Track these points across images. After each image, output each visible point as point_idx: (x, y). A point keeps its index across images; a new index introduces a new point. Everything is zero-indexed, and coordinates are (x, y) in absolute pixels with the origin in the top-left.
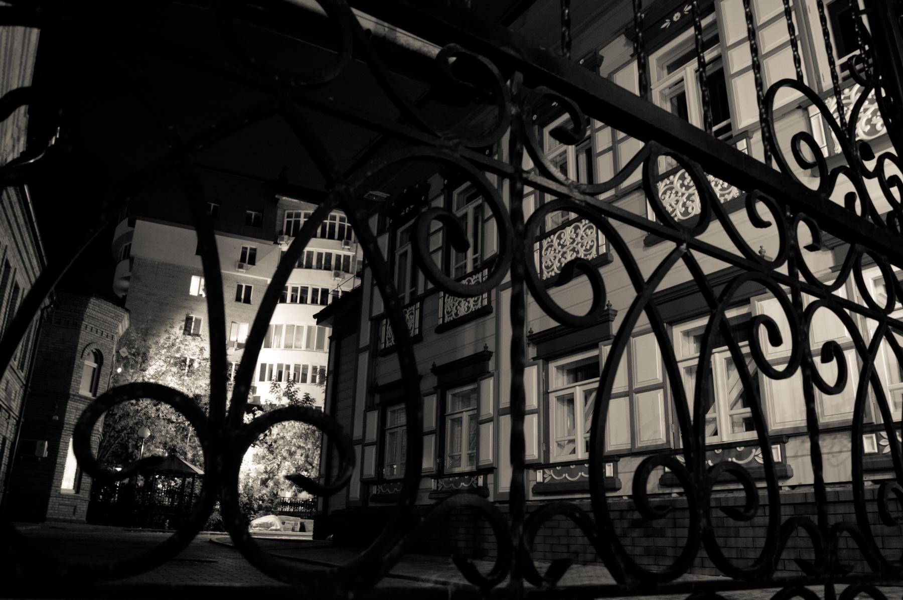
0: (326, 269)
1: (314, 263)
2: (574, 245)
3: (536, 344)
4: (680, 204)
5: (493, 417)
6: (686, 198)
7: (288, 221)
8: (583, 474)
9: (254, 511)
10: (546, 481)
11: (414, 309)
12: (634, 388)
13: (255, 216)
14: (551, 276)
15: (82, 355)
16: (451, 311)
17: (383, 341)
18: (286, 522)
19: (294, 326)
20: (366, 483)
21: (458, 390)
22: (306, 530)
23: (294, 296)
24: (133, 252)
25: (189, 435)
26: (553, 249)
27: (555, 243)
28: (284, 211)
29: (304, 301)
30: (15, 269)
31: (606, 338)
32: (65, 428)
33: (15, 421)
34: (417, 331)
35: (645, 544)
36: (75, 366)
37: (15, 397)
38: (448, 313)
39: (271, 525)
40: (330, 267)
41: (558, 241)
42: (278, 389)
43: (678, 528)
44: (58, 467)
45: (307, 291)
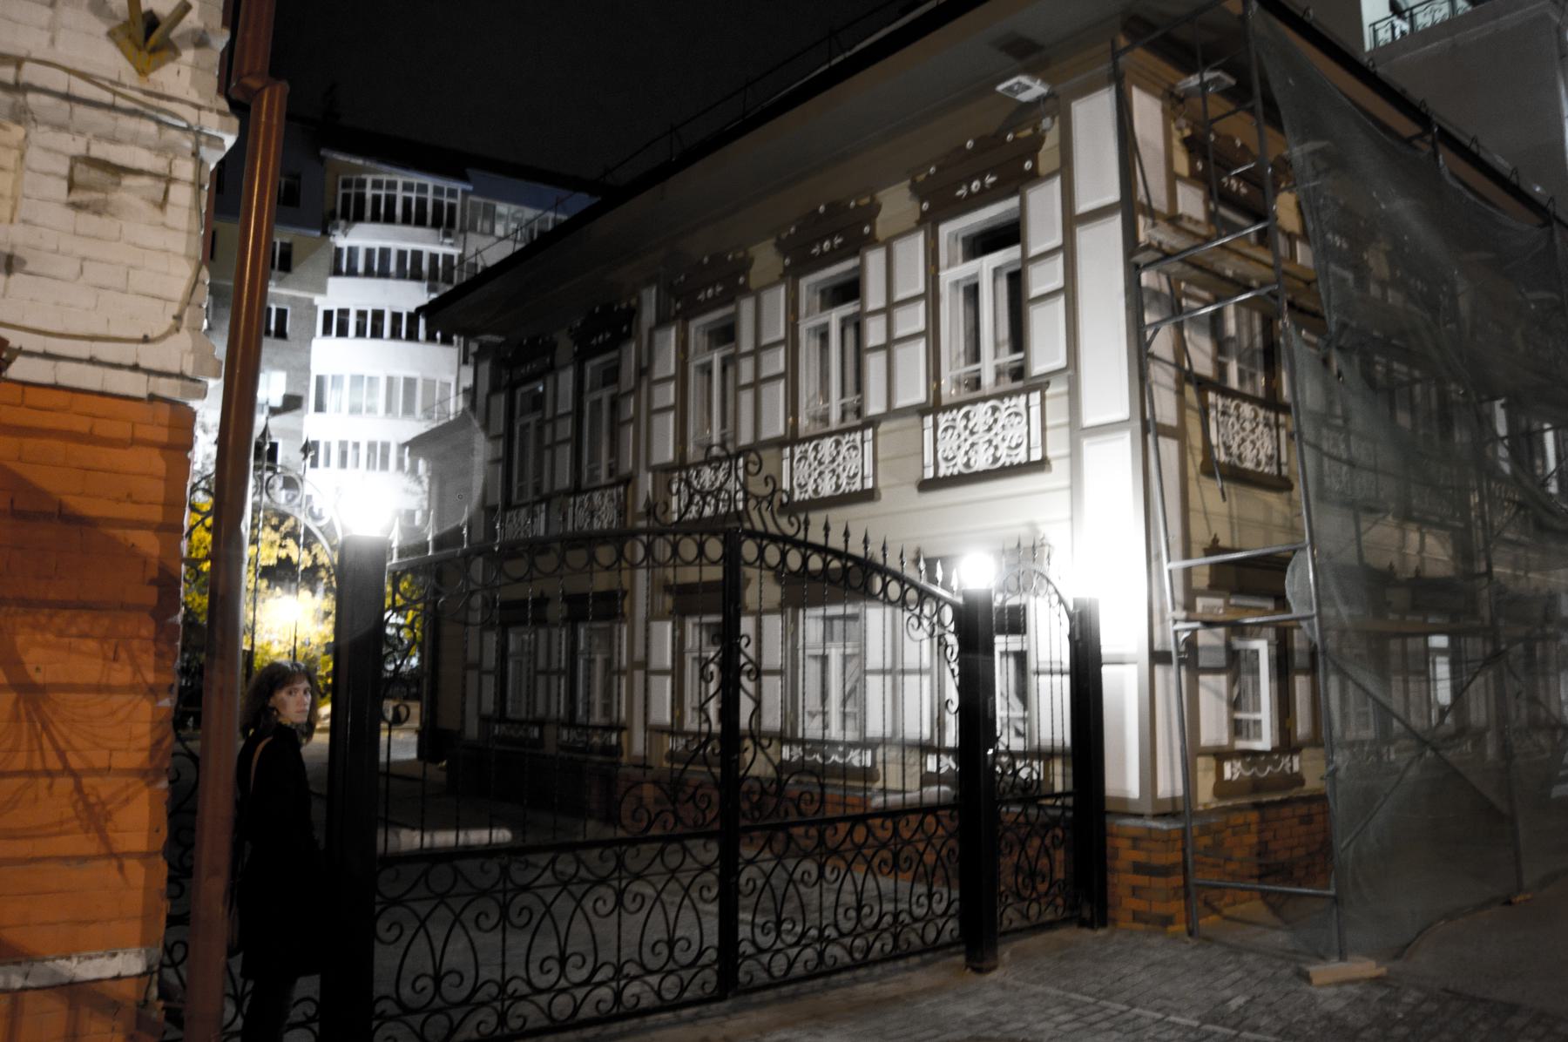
1: (393, 267)
19: (363, 377)
20: (485, 720)
23: (362, 325)
28: (337, 176)
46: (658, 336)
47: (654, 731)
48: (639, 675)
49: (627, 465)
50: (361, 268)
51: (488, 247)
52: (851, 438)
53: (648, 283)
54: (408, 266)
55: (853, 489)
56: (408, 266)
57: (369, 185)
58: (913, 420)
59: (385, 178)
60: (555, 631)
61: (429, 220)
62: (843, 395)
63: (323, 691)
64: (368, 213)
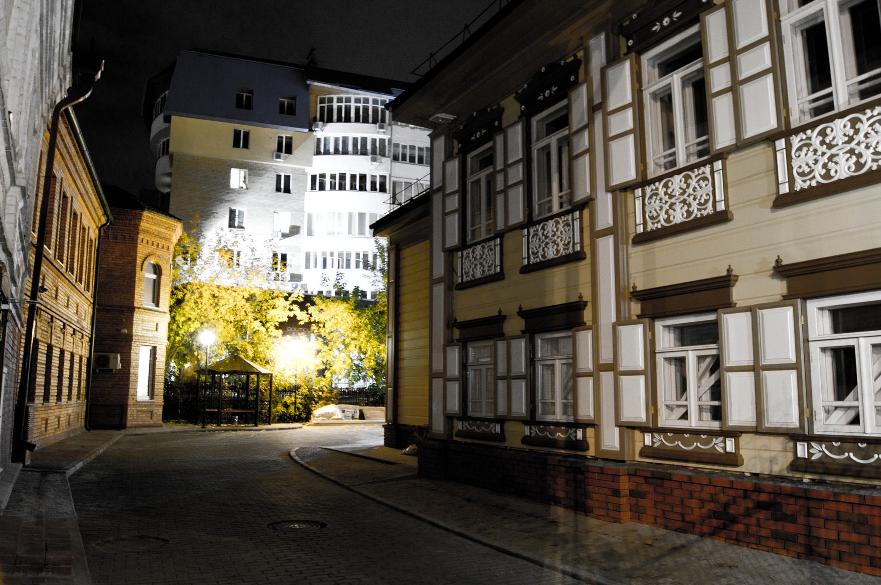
0: (362, 154)
1: (350, 148)
2: (685, 196)
3: (641, 300)
4: (820, 164)
5: (593, 372)
6: (828, 159)
7: (321, 107)
8: (699, 444)
9: (314, 401)
10: (655, 445)
11: (493, 245)
12: (761, 365)
13: (288, 103)
14: (657, 228)
15: (142, 268)
16: (537, 252)
17: (459, 274)
18: (346, 410)
20: (449, 418)
21: (549, 336)
22: (365, 417)
23: (333, 183)
24: (171, 149)
25: (248, 333)
26: (658, 198)
27: (661, 191)
28: (317, 97)
29: (343, 188)
30: (72, 198)
31: (725, 306)
32: (134, 340)
33: (87, 338)
34: (498, 269)
35: (773, 527)
36: (136, 280)
37: (85, 317)
38: (534, 253)
39: (333, 414)
40: (367, 152)
41: (665, 190)
42: (328, 283)
43: (812, 517)
44: (132, 378)
45: (345, 177)
46: (611, 73)
47: (628, 428)
48: (607, 378)
49: (583, 191)
50: (332, 150)
51: (435, 60)
52: (700, 172)
53: (596, 32)
54: (359, 147)
55: (705, 213)
56: (359, 147)
57: (335, 100)
58: (761, 150)
59: (344, 96)
60: (514, 343)
61: (370, 119)
62: (561, 190)
63: (316, 399)
64: (335, 117)
